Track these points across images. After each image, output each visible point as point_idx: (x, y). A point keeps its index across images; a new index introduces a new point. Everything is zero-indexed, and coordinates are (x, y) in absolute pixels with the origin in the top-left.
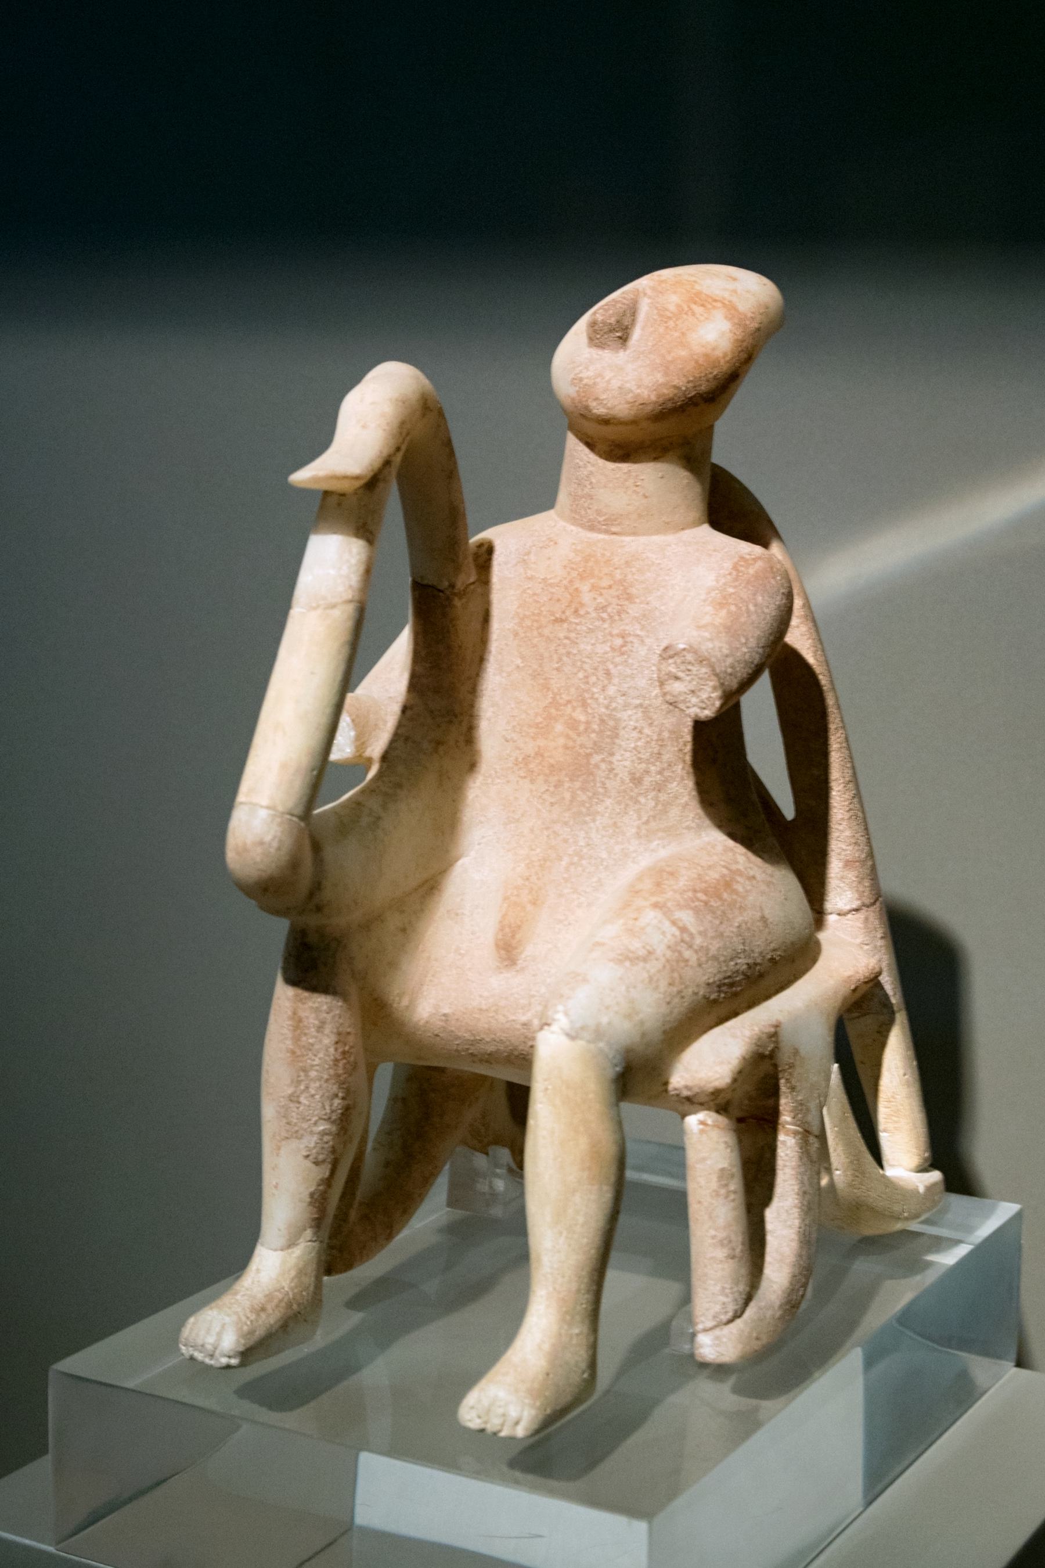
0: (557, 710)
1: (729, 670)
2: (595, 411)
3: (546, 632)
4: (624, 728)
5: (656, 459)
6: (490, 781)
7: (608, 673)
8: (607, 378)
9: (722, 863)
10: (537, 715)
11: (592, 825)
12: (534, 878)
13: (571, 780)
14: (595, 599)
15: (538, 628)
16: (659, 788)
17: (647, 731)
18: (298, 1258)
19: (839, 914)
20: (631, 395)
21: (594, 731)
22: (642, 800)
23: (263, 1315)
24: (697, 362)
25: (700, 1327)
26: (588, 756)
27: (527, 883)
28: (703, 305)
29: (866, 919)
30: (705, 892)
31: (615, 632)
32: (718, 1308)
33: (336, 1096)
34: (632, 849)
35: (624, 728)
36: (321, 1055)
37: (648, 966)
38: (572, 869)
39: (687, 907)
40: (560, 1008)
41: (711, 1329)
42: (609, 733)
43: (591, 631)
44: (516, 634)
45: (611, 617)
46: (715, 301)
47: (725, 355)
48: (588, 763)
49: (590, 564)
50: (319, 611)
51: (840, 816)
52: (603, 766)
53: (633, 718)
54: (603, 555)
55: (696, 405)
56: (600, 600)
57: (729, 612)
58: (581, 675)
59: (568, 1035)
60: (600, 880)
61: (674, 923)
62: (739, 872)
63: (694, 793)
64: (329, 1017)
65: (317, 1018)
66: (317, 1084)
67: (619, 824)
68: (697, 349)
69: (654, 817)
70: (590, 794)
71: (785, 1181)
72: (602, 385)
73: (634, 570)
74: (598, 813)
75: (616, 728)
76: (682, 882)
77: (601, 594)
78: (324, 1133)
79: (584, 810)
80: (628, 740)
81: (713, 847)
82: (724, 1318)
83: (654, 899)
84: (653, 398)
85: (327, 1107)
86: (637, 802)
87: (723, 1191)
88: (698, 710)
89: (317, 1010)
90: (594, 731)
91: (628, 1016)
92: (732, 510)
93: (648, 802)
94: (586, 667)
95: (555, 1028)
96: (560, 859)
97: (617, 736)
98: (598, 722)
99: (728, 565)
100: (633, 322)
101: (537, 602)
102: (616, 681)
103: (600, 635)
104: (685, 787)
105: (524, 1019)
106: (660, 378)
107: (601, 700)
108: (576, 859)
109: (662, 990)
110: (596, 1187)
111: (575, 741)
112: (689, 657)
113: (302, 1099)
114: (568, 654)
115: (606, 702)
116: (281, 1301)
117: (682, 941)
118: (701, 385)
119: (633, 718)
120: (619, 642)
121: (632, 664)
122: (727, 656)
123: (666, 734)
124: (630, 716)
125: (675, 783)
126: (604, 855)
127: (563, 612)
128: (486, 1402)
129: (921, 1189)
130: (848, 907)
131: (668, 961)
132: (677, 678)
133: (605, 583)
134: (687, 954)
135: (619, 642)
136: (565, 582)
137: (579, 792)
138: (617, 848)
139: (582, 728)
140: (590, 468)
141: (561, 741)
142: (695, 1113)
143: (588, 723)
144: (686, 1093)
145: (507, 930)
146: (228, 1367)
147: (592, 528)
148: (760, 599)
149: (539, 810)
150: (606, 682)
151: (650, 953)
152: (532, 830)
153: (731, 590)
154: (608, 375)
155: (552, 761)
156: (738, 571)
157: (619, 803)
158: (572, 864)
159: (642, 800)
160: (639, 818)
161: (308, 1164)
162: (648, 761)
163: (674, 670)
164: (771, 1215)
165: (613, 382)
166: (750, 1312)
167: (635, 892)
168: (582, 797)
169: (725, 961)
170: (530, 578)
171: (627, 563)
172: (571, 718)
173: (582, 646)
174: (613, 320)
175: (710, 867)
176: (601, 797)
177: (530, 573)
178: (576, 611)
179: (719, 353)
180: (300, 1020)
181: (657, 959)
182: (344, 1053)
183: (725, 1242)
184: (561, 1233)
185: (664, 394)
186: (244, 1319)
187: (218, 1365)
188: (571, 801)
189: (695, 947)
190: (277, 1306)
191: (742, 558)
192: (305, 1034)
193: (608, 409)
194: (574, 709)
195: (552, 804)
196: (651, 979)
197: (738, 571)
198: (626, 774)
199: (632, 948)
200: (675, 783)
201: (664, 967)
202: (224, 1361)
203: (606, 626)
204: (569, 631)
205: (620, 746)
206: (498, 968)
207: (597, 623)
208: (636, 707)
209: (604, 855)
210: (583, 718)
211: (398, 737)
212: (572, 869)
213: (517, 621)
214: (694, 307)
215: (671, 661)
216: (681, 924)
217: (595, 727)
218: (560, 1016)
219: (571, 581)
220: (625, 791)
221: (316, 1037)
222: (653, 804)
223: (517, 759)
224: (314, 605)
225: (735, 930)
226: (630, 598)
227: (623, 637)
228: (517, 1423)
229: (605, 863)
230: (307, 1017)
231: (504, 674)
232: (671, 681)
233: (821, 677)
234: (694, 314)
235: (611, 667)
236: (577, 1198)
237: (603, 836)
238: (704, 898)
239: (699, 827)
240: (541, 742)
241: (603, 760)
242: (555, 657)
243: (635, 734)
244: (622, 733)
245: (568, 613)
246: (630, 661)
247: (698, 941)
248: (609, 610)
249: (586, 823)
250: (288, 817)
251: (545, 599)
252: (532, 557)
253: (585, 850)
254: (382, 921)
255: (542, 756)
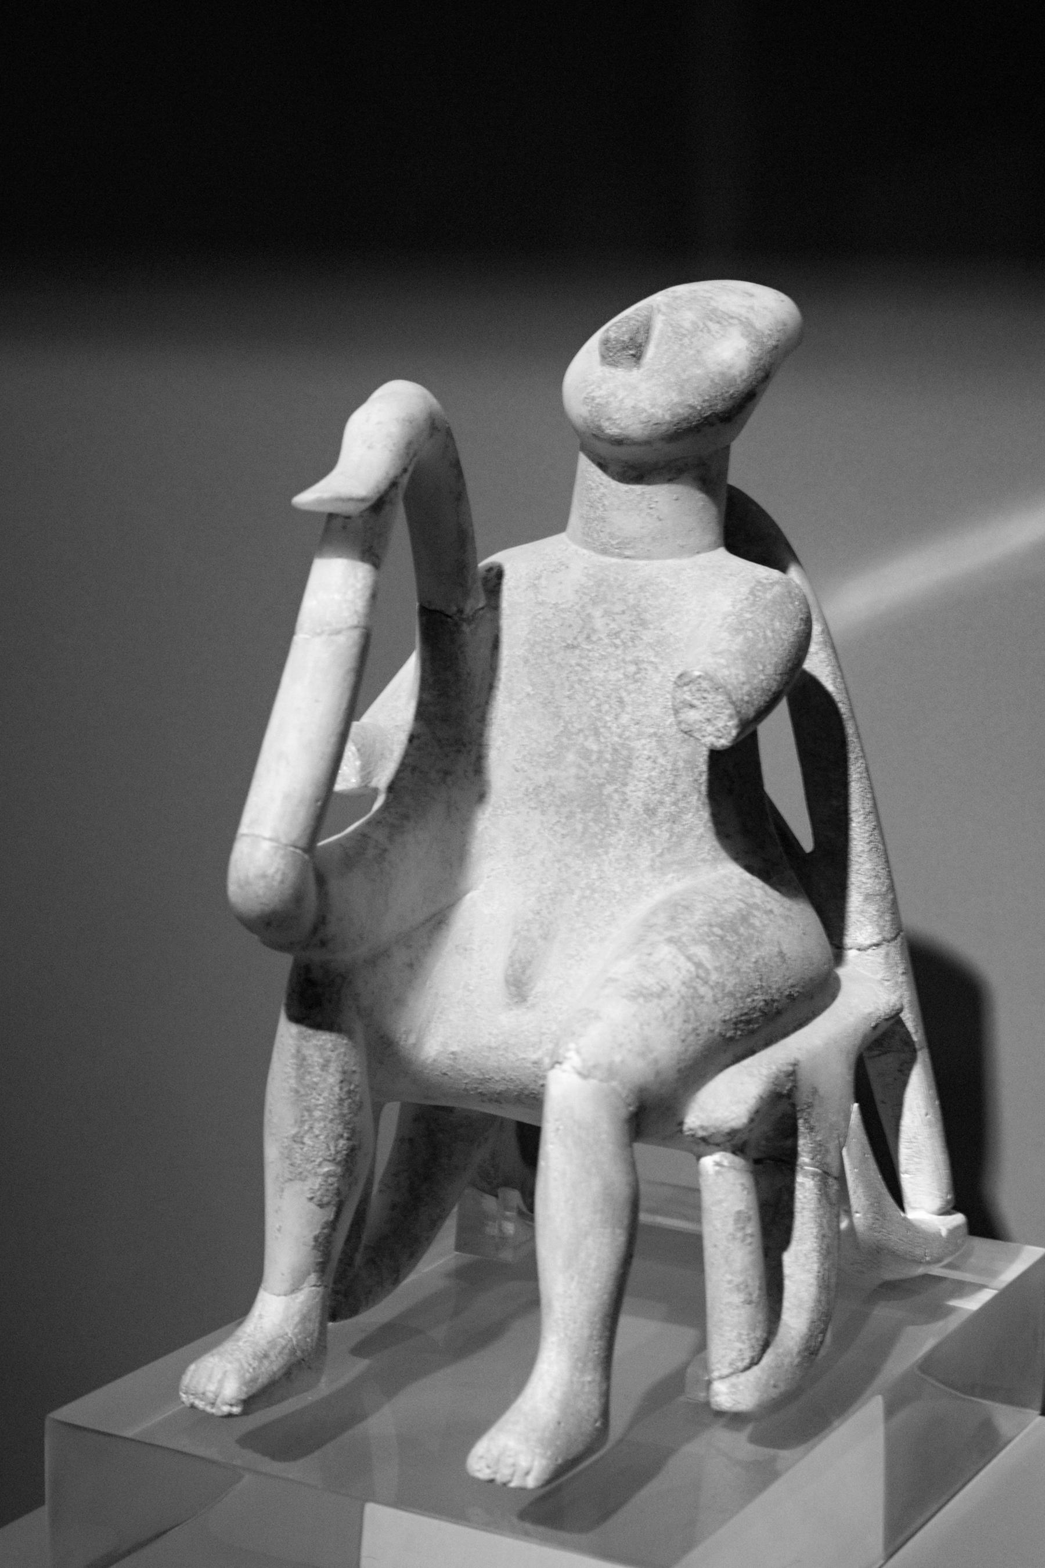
0: (569, 739)
1: (746, 698)
2: (608, 431)
3: (557, 658)
4: (637, 758)
5: (670, 481)
6: (499, 811)
7: (621, 701)
8: (620, 397)
9: (739, 897)
10: (548, 744)
11: (604, 857)
12: (544, 912)
13: (583, 811)
14: (608, 624)
15: (549, 655)
16: (674, 819)
17: (661, 761)
18: (302, 1303)
19: (859, 949)
20: (644, 415)
21: (606, 761)
22: (656, 831)
23: (266, 1363)
24: (712, 381)
25: (716, 1374)
26: (601, 786)
27: (537, 917)
28: (718, 322)
29: (887, 954)
30: (721, 926)
31: (628, 658)
32: (734, 1355)
33: (341, 1136)
34: (645, 882)
35: (637, 758)
36: (326, 1094)
37: (662, 1002)
38: (584, 903)
39: (703, 942)
40: (572, 1046)
41: (727, 1376)
42: (622, 763)
43: (603, 657)
44: (526, 661)
45: (624, 643)
46: (732, 318)
47: (742, 373)
48: (601, 794)
49: (603, 589)
50: (324, 637)
51: (860, 848)
52: (616, 796)
53: (648, 747)
54: (616, 579)
55: (712, 425)
56: (613, 625)
57: (746, 638)
58: (593, 703)
59: (580, 1074)
60: (613, 914)
61: (689, 958)
62: (756, 906)
63: (710, 824)
64: (334, 1055)
65: (321, 1056)
66: (322, 1124)
67: (633, 857)
68: (714, 368)
69: (669, 849)
70: (603, 826)
71: (803, 1224)
72: (615, 404)
73: (647, 594)
74: (611, 844)
75: (629, 757)
76: (698, 916)
77: (614, 620)
78: (328, 1175)
79: (597, 842)
80: (642, 770)
81: (730, 880)
82: (741, 1365)
83: (668, 934)
84: (668, 417)
85: (332, 1148)
86: (651, 834)
87: (739, 1235)
88: (714, 740)
89: (321, 1048)
90: (606, 761)
91: (642, 1055)
92: (749, 534)
93: (662, 834)
94: (599, 694)
95: (566, 1066)
96: (572, 892)
97: (630, 766)
98: (611, 751)
99: (745, 590)
100: (647, 339)
101: (547, 627)
102: (629, 709)
103: (613, 661)
104: (700, 818)
105: (534, 1057)
106: (675, 397)
107: (614, 729)
108: (588, 893)
109: (677, 1027)
110: (608, 1230)
111: (586, 771)
112: (705, 684)
113: (306, 1140)
114: (580, 681)
115: (619, 731)
116: (284, 1348)
117: (698, 977)
118: (717, 405)
119: (648, 747)
120: (632, 669)
121: (646, 692)
122: (743, 683)
123: (681, 764)
124: (644, 745)
125: (690, 815)
126: (617, 889)
127: (575, 638)
128: (495, 1452)
129: (944, 1233)
130: (868, 942)
131: (683, 997)
132: (692, 706)
133: (618, 608)
134: (703, 990)
135: (632, 669)
136: (577, 607)
137: (591, 824)
138: (631, 882)
139: (594, 757)
140: (602, 490)
141: (573, 771)
142: (710, 1154)
143: (600, 752)
144: (701, 1133)
145: (517, 966)
146: (230, 1415)
147: (604, 552)
148: (777, 624)
149: (550, 842)
150: (619, 710)
151: (664, 989)
152: (543, 863)
153: (748, 616)
154: (621, 394)
155: (563, 791)
156: (755, 596)
157: (633, 835)
158: (584, 897)
159: (656, 831)
160: (653, 850)
161: (312, 1206)
162: (662, 792)
163: (689, 698)
164: (788, 1258)
165: (626, 401)
166: (768, 1359)
167: (648, 926)
168: (595, 828)
169: (741, 998)
170: (542, 603)
171: (641, 588)
172: (583, 747)
173: (594, 674)
174: (626, 338)
175: (726, 901)
176: (613, 828)
177: (540, 598)
178: (588, 637)
179: (735, 372)
180: (304, 1059)
181: (671, 996)
182: (349, 1092)
183: (742, 1287)
184: (572, 1278)
185: (679, 414)
186: (246, 1366)
187: (220, 1414)
188: (583, 833)
189: (711, 983)
190: (280, 1353)
191: (759, 582)
192: (309, 1073)
193: (621, 429)
194: (586, 738)
195: (564, 836)
196: (665, 1016)
197: (755, 596)
198: (640, 805)
199: (646, 984)
200: (690, 815)
201: (679, 1003)
202: (226, 1409)
203: (619, 652)
204: (581, 658)
205: (634, 776)
206: (508, 1004)
207: (610, 650)
208: (650, 736)
209: (617, 889)
210: (595, 747)
211: (405, 767)
212: (584, 903)
213: (527, 647)
214: (710, 324)
215: (686, 688)
216: (696, 960)
217: (608, 756)
218: (571, 1054)
219: (583, 607)
220: (638, 823)
221: (320, 1076)
222: (668, 835)
223: (527, 790)
224: (318, 631)
225: (752, 965)
226: (644, 623)
227: (636, 664)
228: (527, 1473)
229: (618, 897)
230: (311, 1056)
231: (514, 702)
232: (686, 710)
233: (840, 705)
234: (709, 331)
235: (624, 694)
236: (590, 1241)
237: (616, 869)
238: (719, 932)
239: (715, 859)
240: (552, 772)
241: (616, 791)
242: (567, 684)
243: (649, 764)
244: (635, 762)
245: (580, 639)
246: (644, 688)
247: (714, 977)
248: (622, 636)
249: (598, 855)
250: (292, 849)
251: (557, 624)
252: (543, 582)
253: (597, 883)
254: (389, 956)
255: (553, 786)
